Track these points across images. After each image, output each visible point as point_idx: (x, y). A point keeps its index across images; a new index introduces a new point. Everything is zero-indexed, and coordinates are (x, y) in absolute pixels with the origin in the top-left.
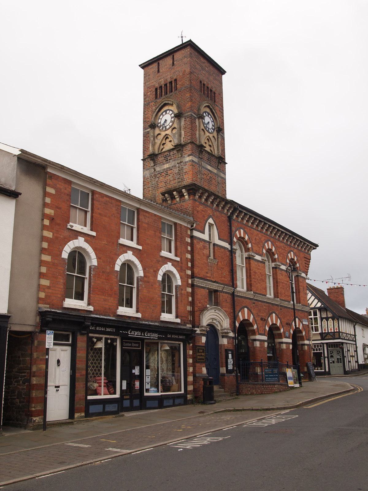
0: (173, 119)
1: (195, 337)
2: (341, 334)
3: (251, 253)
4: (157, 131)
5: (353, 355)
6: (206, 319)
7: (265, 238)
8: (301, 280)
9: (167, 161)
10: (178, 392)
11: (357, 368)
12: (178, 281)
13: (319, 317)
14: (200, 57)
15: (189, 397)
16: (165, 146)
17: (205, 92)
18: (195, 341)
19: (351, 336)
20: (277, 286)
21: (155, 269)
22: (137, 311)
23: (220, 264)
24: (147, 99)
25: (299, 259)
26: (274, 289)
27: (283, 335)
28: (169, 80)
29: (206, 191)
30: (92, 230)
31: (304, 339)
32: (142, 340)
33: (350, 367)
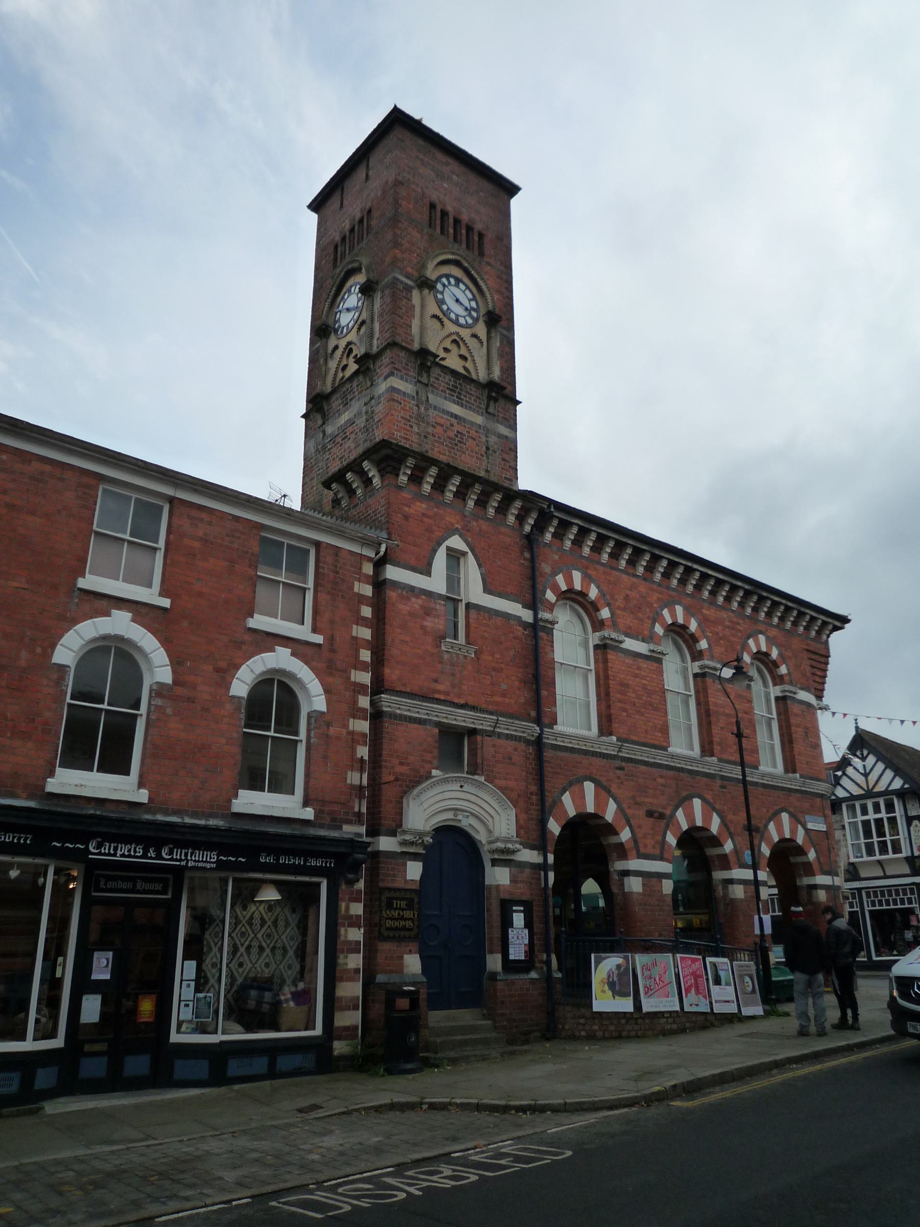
6: (422, 813)
8: (795, 709)
10: (306, 1029)
13: (901, 816)
14: (433, 150)
15: (340, 1047)
20: (709, 723)
21: (223, 664)
26: (700, 733)
27: (732, 859)
31: (813, 871)
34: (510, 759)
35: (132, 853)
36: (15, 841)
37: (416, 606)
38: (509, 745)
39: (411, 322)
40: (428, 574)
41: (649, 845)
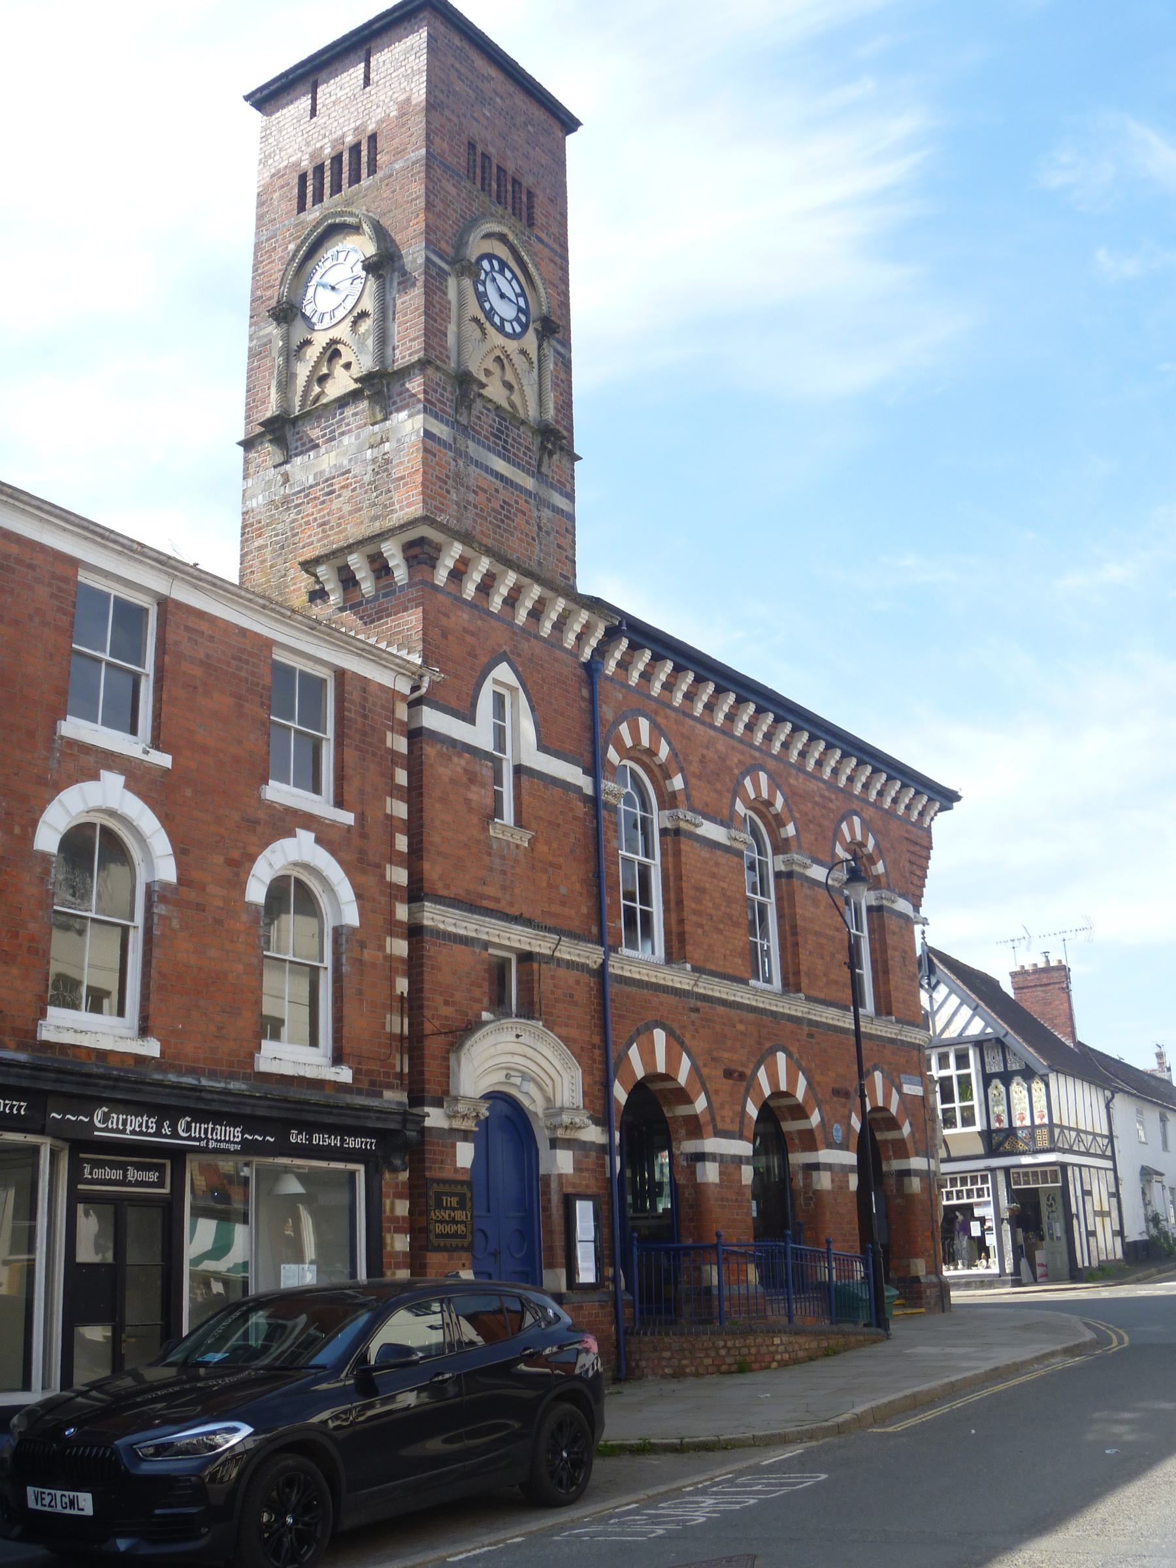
2: (1057, 1131)
5: (1106, 1208)
7: (741, 757)
8: (892, 924)
11: (1119, 1255)
13: (977, 1074)
17: (490, 185)
18: (423, 1160)
19: (1094, 1138)
20: (796, 945)
21: (236, 854)
22: (144, 1031)
23: (542, 848)
25: (886, 844)
28: (350, 139)
33: (1094, 1254)
34: (572, 996)
35: (144, 1129)
36: (7, 1111)
37: (458, 769)
38: (572, 976)
39: (446, 328)
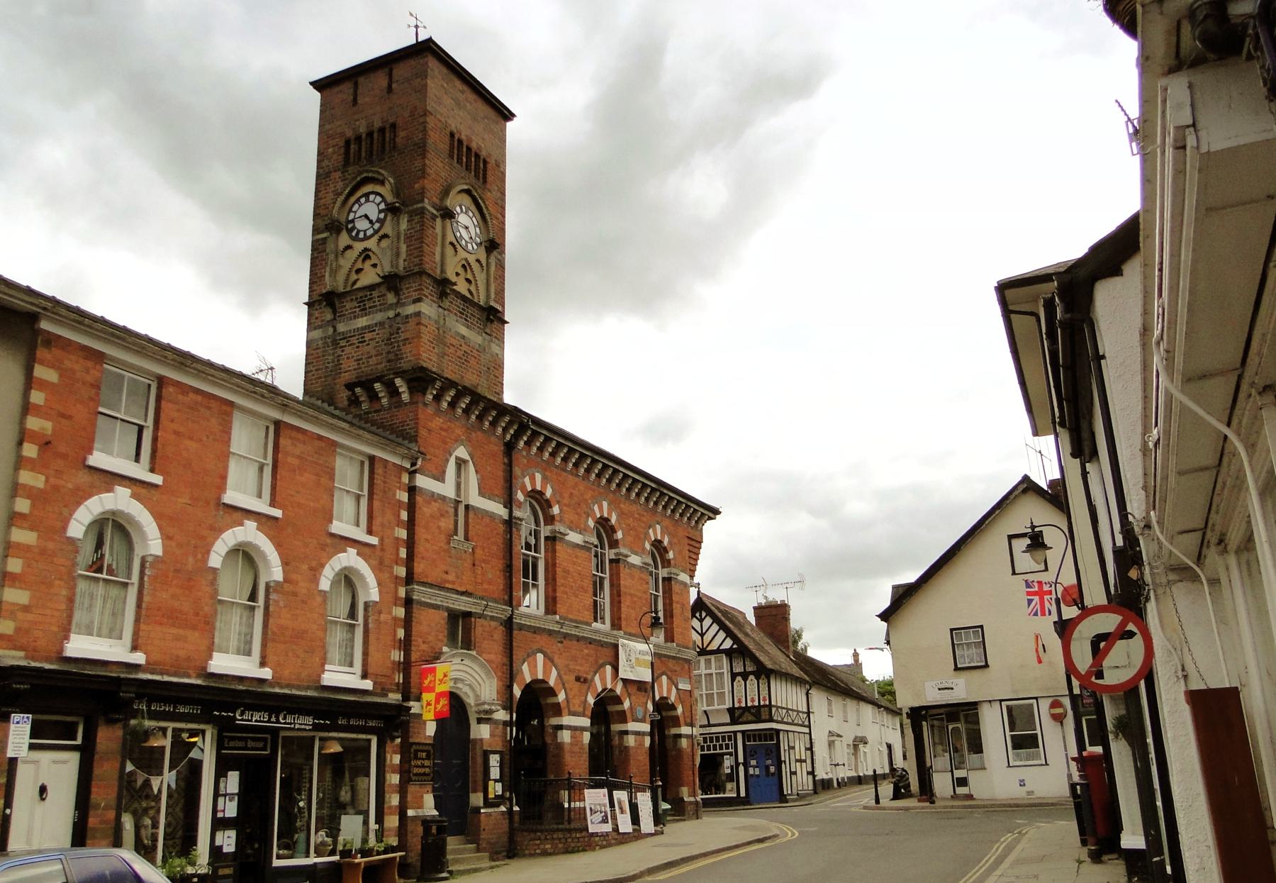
0: (382, 216)
1: (408, 722)
2: (774, 710)
3: (559, 527)
4: (344, 239)
8: (676, 588)
9: (364, 311)
11: (811, 787)
12: (371, 591)
14: (453, 77)
16: (361, 276)
18: (408, 732)
21: (314, 564)
22: (263, 664)
24: (326, 163)
27: (629, 715)
28: (377, 124)
29: (451, 384)
30: (152, 470)
32: (274, 732)
40: (443, 481)
41: (576, 705)
